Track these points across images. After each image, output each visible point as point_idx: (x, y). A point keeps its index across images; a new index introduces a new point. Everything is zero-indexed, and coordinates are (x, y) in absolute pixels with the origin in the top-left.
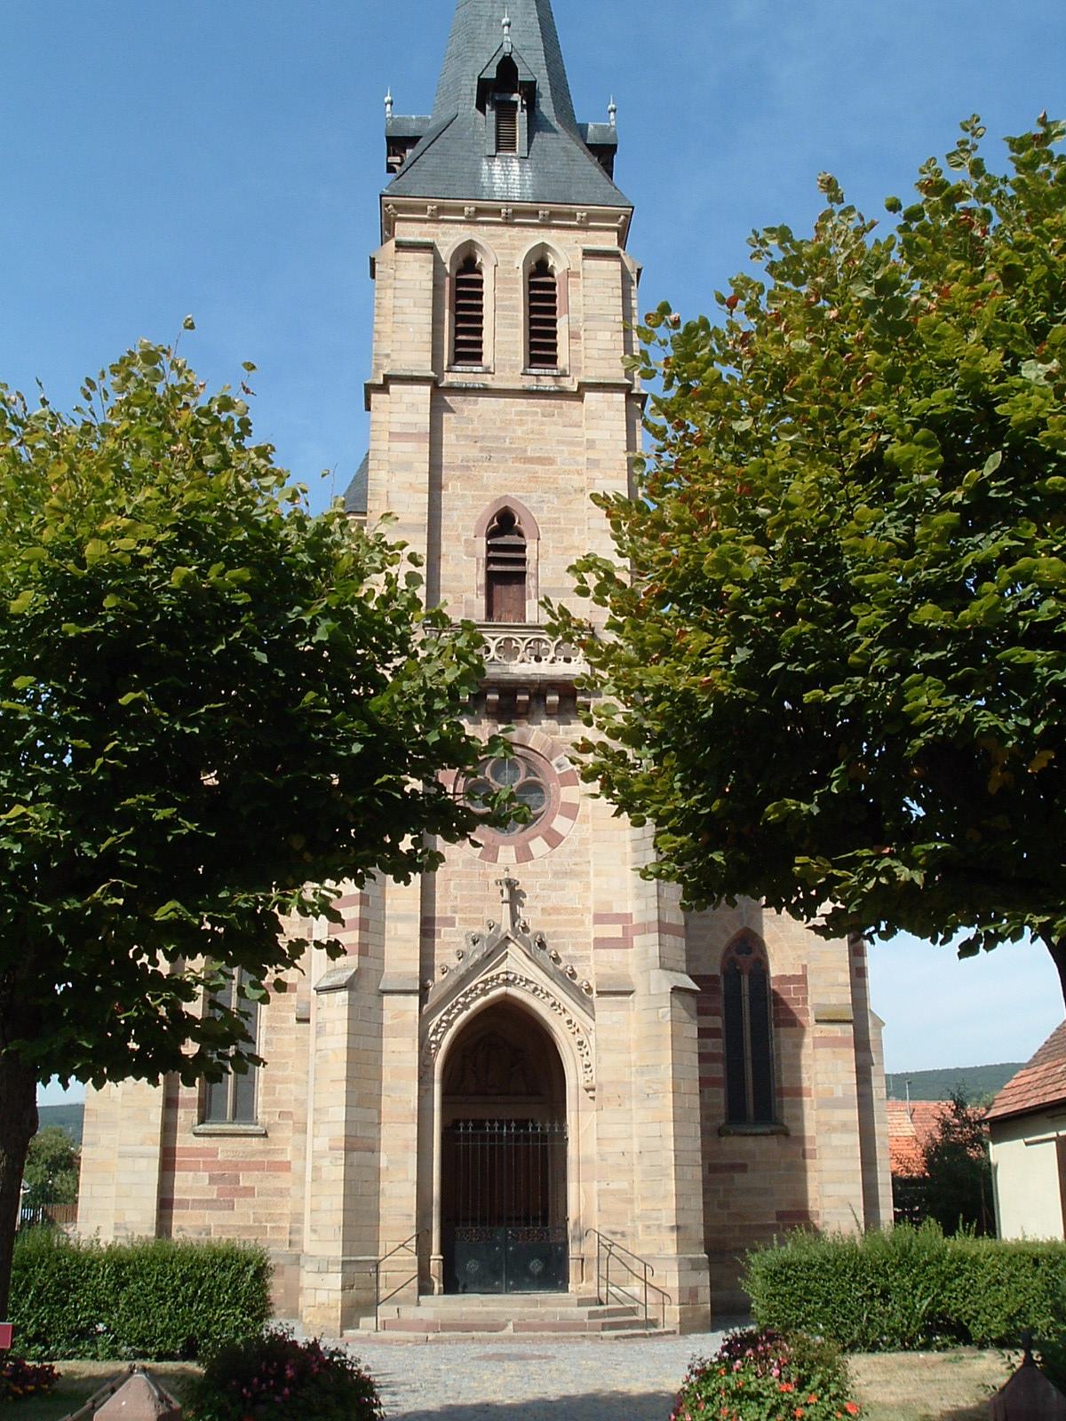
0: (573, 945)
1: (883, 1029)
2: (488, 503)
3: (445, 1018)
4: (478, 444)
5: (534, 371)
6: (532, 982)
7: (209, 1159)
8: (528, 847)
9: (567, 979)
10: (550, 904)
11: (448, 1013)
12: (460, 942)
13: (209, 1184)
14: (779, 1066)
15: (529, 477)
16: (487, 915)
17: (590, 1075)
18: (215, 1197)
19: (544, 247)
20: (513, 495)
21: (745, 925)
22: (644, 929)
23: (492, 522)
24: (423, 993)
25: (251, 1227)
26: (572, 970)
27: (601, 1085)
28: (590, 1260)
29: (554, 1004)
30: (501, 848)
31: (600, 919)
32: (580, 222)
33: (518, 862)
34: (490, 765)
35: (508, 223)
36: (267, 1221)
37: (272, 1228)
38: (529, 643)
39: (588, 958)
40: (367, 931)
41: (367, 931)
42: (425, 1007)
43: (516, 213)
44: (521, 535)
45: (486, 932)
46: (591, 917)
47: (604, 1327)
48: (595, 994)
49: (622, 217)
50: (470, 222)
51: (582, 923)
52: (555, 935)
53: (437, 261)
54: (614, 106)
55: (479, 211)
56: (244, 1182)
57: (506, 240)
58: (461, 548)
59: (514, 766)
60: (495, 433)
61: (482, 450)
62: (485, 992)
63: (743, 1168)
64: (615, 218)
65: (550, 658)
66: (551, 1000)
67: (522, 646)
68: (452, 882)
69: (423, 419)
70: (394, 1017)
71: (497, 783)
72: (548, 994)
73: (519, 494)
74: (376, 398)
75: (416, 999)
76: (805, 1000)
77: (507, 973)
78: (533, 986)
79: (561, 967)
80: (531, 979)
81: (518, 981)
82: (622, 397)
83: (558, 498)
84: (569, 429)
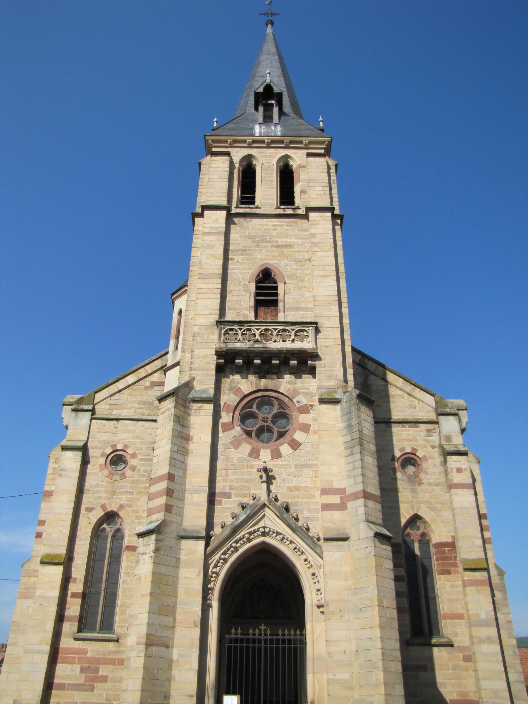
0: (308, 510)
3: (222, 557)
4: (252, 240)
5: (282, 207)
6: (280, 534)
7: (81, 656)
8: (279, 451)
10: (293, 484)
11: (225, 553)
12: (234, 508)
15: (280, 254)
16: (253, 491)
17: (321, 596)
18: (82, 682)
20: (270, 262)
21: (415, 512)
22: (355, 496)
23: (258, 275)
24: (208, 538)
26: (307, 525)
27: (327, 603)
29: (295, 548)
31: (325, 492)
32: (305, 145)
34: (256, 403)
35: (268, 147)
36: (114, 700)
38: (279, 331)
39: (318, 518)
40: (172, 496)
41: (172, 496)
42: (209, 549)
43: (273, 142)
44: (275, 282)
45: (251, 502)
46: (319, 492)
48: (322, 540)
49: (326, 142)
50: (250, 147)
51: (314, 496)
52: (296, 504)
53: (232, 163)
54: (322, 119)
56: (101, 673)
57: (268, 154)
58: (242, 288)
59: (270, 404)
60: (261, 234)
62: (249, 540)
64: (323, 143)
65: (291, 339)
66: (293, 546)
67: (275, 333)
68: (230, 471)
69: (222, 225)
70: (187, 555)
71: (259, 413)
72: (291, 542)
74: (197, 220)
75: (202, 543)
76: (455, 558)
77: (264, 527)
78: (281, 536)
79: (300, 523)
80: (280, 531)
81: (271, 533)
82: (329, 215)
83: (296, 263)
84: (302, 232)
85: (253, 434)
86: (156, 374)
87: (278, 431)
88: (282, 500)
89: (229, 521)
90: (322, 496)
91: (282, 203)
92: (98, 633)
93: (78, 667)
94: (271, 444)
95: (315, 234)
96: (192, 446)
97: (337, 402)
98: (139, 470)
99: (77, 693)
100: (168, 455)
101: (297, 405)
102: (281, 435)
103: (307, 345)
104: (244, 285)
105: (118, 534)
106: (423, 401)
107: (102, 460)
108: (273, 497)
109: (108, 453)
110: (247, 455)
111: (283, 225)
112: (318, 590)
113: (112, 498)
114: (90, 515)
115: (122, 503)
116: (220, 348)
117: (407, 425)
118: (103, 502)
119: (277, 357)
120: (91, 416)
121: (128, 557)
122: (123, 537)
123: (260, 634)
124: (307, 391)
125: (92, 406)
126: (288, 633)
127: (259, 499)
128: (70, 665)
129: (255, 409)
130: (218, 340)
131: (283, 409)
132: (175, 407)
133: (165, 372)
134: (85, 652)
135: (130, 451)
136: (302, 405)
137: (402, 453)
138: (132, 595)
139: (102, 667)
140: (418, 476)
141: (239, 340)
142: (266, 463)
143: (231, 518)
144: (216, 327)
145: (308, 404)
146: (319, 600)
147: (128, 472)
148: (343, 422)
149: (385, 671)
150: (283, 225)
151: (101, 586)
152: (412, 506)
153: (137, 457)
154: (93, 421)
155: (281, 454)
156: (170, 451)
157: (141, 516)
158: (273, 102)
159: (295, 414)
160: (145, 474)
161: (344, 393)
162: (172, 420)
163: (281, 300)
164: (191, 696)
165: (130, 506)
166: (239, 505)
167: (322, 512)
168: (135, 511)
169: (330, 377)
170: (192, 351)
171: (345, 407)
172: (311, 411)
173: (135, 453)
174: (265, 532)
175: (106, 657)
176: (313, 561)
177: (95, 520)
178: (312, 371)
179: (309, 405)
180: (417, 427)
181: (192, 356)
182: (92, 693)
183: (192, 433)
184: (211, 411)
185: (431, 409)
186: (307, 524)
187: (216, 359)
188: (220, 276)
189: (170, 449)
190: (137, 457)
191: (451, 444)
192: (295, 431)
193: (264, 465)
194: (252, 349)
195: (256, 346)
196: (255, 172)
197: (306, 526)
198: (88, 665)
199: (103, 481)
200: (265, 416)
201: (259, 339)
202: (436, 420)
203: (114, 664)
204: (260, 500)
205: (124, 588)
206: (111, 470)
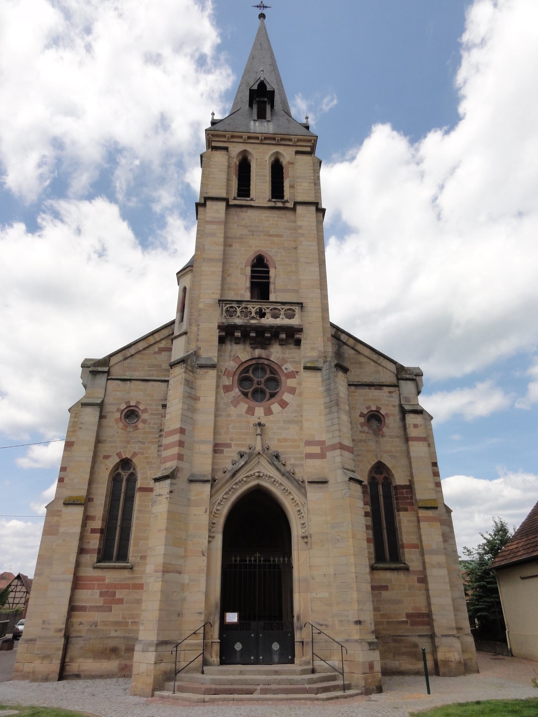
1: (452, 514)
2: (252, 253)
5: (273, 200)
6: (272, 477)
9: (290, 476)
11: (227, 493)
14: (401, 532)
16: (248, 442)
18: (101, 604)
19: (277, 153)
20: (263, 249)
21: (379, 460)
28: (308, 643)
29: (284, 489)
30: (257, 408)
31: (309, 443)
33: (265, 415)
34: (252, 367)
36: (129, 619)
37: (132, 622)
41: (183, 447)
42: (213, 491)
43: (266, 138)
44: (267, 266)
45: (248, 451)
46: (303, 443)
47: (318, 691)
48: (306, 483)
55: (249, 138)
61: (249, 231)
63: (386, 588)
66: (283, 488)
73: (266, 249)
74: (200, 209)
77: (259, 472)
78: (273, 480)
80: (272, 476)
85: (250, 395)
86: (164, 342)
87: (269, 393)
88: (273, 449)
89: (229, 467)
90: (306, 447)
91: (273, 197)
92: (115, 562)
93: (97, 592)
94: (264, 403)
95: (301, 226)
96: (200, 405)
97: (317, 369)
98: (150, 423)
99: (97, 613)
100: (180, 412)
101: (285, 371)
102: (272, 395)
103: (294, 322)
104: (241, 269)
105: (132, 479)
106: (386, 368)
107: (118, 415)
108: (266, 447)
109: (123, 409)
110: (244, 412)
111: (274, 217)
112: (303, 524)
113: (126, 447)
114: (107, 461)
115: (135, 451)
116: (223, 323)
117: (373, 388)
118: (119, 450)
119: (268, 331)
120: (108, 377)
121: (140, 497)
122: (135, 480)
123: (255, 561)
125: (108, 368)
126: (277, 560)
127: (255, 449)
129: (250, 374)
130: (220, 316)
131: (274, 374)
132: (185, 373)
133: (172, 340)
134: (103, 579)
135: (141, 407)
136: (289, 371)
137: (369, 411)
138: (88, 542)
139: (118, 591)
140: (381, 430)
141: (238, 317)
142: (260, 419)
143: (231, 465)
144: (218, 305)
145: (294, 371)
146: (303, 533)
147: (140, 425)
148: (323, 386)
149: (358, 590)
150: (274, 217)
151: (117, 522)
152: (376, 455)
153: (148, 412)
154: (109, 382)
155: (272, 412)
156: (181, 410)
157: (152, 462)
158: (266, 99)
159: (283, 378)
160: (155, 426)
161: (324, 362)
162: (183, 383)
163: (272, 283)
164: (200, 613)
165: (142, 453)
166: (238, 454)
167: (306, 460)
168: (147, 458)
169: (312, 349)
171: (324, 374)
172: (297, 376)
173: (146, 408)
174: (259, 476)
175: (122, 583)
176: (299, 500)
177: (112, 466)
178: (298, 343)
179: (295, 371)
180: (381, 389)
181: (198, 329)
182: (111, 613)
183: (199, 394)
184: (215, 375)
185: (392, 374)
186: (294, 469)
187: (219, 332)
188: (221, 261)
189: (181, 407)
190: (148, 412)
191: (409, 404)
192: (283, 393)
193: (259, 421)
194: (249, 324)
195: (253, 321)
196: (249, 166)
197: (293, 471)
198: (106, 590)
200: (259, 380)
201: (255, 316)
202: (397, 384)
203: (129, 588)
204: (255, 449)
205: (138, 523)
206: (125, 423)
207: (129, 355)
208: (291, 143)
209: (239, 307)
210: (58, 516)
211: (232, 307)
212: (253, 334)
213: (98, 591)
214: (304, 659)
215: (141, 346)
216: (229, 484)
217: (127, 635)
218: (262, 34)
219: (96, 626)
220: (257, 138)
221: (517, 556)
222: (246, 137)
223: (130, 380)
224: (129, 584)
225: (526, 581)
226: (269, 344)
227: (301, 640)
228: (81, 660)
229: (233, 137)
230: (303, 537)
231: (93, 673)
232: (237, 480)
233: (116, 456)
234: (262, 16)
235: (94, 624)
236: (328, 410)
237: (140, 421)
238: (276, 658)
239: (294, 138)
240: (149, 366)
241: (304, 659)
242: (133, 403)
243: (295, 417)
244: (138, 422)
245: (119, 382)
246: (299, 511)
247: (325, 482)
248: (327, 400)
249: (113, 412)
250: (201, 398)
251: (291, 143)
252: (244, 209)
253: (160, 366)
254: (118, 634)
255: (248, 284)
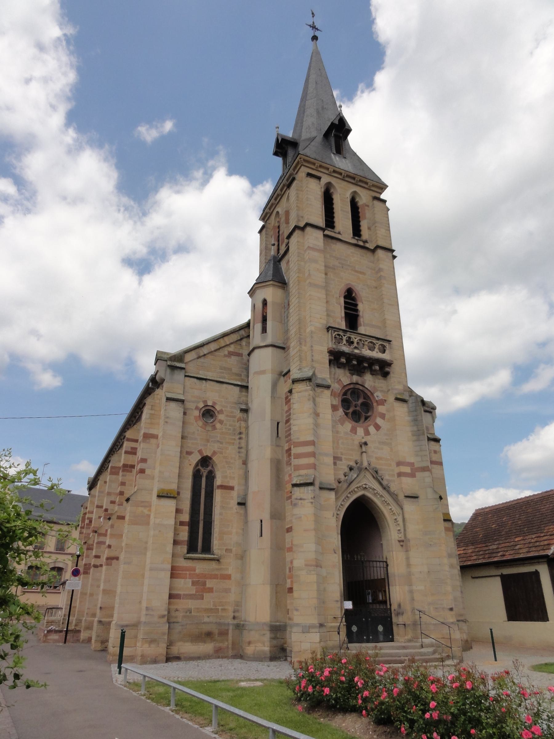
11: (343, 501)
13: (192, 585)
18: (194, 593)
20: (352, 283)
25: (211, 609)
30: (358, 428)
36: (219, 606)
37: (222, 609)
55: (334, 171)
56: (208, 585)
61: (339, 263)
72: (381, 496)
77: (365, 484)
86: (232, 346)
93: (189, 581)
99: (190, 601)
103: (385, 356)
105: (211, 477)
107: (197, 413)
114: (190, 457)
118: (200, 448)
124: (382, 389)
127: (362, 464)
128: (183, 580)
141: (344, 345)
159: (375, 404)
164: (337, 601)
165: (221, 453)
169: (399, 383)
170: (312, 346)
174: (366, 488)
178: (385, 375)
199: (198, 431)
203: (217, 578)
205: (222, 519)
207: (202, 354)
208: (366, 186)
209: (344, 336)
210: (142, 506)
211: (339, 335)
212: (355, 362)
213: (190, 580)
214: (406, 638)
215: (213, 347)
216: (345, 493)
217: (218, 621)
218: (316, 56)
219: (191, 612)
220: (341, 174)
221: (470, 560)
222: (332, 170)
223: (206, 380)
224: (216, 575)
225: (475, 580)
226: (364, 372)
227: (403, 623)
228: (179, 644)
229: (321, 166)
230: (399, 541)
231: (192, 655)
232: (350, 490)
233: (198, 453)
234: (315, 38)
235: (189, 610)
236: (415, 438)
237: (216, 421)
238: (381, 637)
239: (331, 169)
240: (221, 368)
241: (406, 638)
242: (210, 403)
243: (386, 439)
244: (215, 422)
245: (195, 380)
246: (396, 519)
247: (416, 497)
248: (415, 429)
249: (192, 409)
250: (321, 415)
251: (366, 186)
252: (334, 241)
253: (230, 369)
254: (211, 619)
255: (343, 315)
